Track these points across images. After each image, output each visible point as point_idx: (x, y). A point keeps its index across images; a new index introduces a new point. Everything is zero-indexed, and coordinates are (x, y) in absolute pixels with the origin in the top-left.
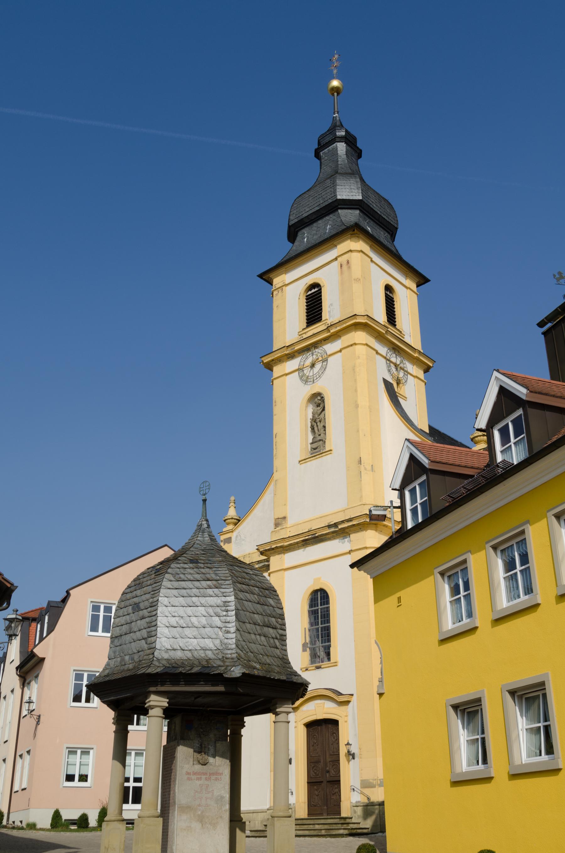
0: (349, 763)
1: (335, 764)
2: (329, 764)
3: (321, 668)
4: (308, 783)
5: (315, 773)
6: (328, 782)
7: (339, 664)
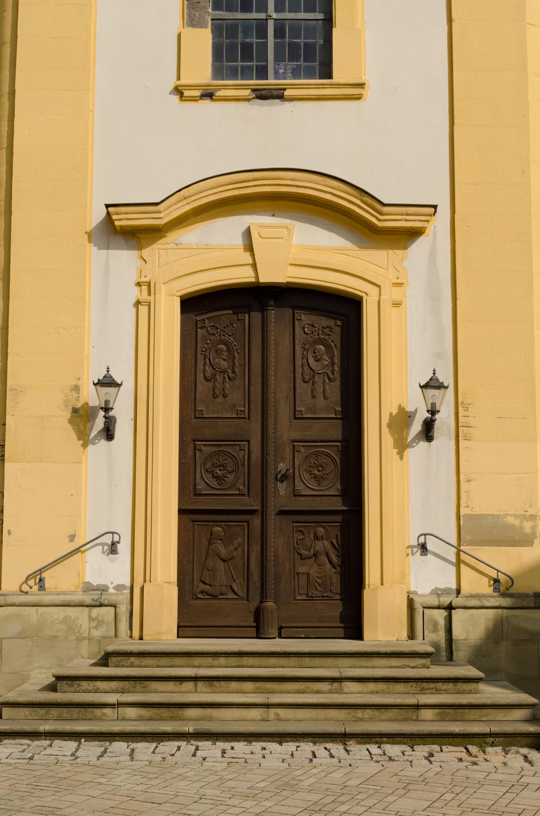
0: (401, 454)
3: (281, 97)
4: (181, 512)
5: (217, 478)
7: (368, 93)
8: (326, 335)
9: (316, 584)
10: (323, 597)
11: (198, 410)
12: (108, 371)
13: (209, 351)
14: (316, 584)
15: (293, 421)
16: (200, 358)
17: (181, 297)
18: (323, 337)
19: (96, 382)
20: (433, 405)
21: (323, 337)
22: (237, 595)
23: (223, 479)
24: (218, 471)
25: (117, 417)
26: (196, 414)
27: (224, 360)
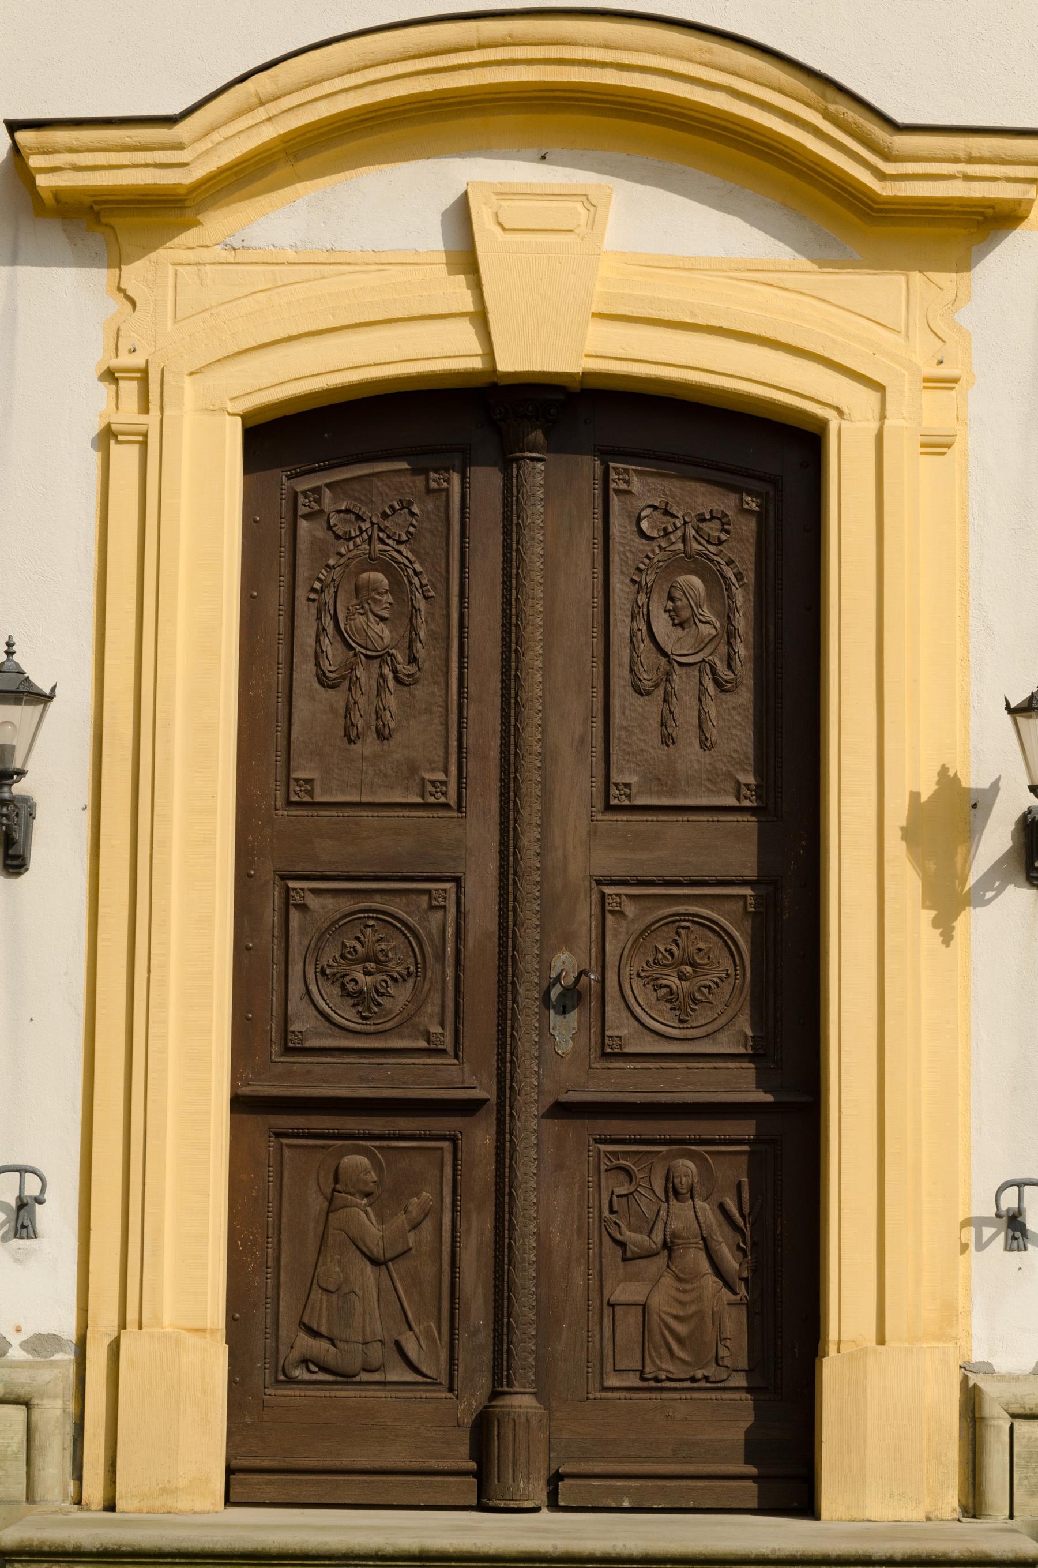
1: (676, 921)
2: (585, 914)
6: (562, 1110)
8: (709, 542)
11: (297, 780)
13: (332, 590)
14: (666, 1333)
17: (245, 417)
18: (700, 548)
21: (700, 548)
23: (374, 1000)
24: (360, 976)
27: (383, 619)
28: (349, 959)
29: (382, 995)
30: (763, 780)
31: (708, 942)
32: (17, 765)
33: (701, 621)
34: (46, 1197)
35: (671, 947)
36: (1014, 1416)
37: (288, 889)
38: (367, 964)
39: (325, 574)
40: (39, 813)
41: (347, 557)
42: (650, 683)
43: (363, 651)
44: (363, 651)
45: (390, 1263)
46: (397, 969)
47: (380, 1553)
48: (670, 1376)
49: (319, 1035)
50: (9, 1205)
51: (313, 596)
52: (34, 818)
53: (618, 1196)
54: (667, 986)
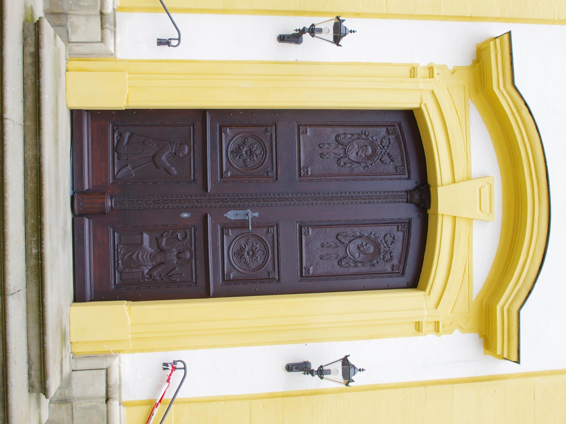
8: (383, 256)
9: (135, 250)
10: (118, 260)
11: (307, 128)
12: (351, 32)
13: (365, 138)
14: (131, 252)
15: (297, 224)
16: (358, 130)
17: (419, 109)
18: (382, 253)
19: (341, 18)
20: (329, 372)
21: (382, 253)
22: (118, 173)
23: (238, 154)
24: (245, 149)
25: (302, 44)
26: (302, 127)
27: (357, 154)
28: (250, 146)
29: (240, 157)
30: (311, 275)
31: (260, 260)
32: (316, 35)
33: (360, 253)
34: (171, 47)
35: (258, 249)
36: (107, 370)
37: (272, 126)
38: (249, 152)
39: (370, 136)
40: (297, 45)
41: (376, 142)
42: (340, 238)
43: (347, 148)
44: (347, 148)
45: (153, 161)
46: (248, 162)
47: (41, 157)
48: (119, 253)
49: (226, 138)
50: (171, 13)
51: (363, 132)
52: (296, 44)
53: (177, 234)
54: (245, 248)
